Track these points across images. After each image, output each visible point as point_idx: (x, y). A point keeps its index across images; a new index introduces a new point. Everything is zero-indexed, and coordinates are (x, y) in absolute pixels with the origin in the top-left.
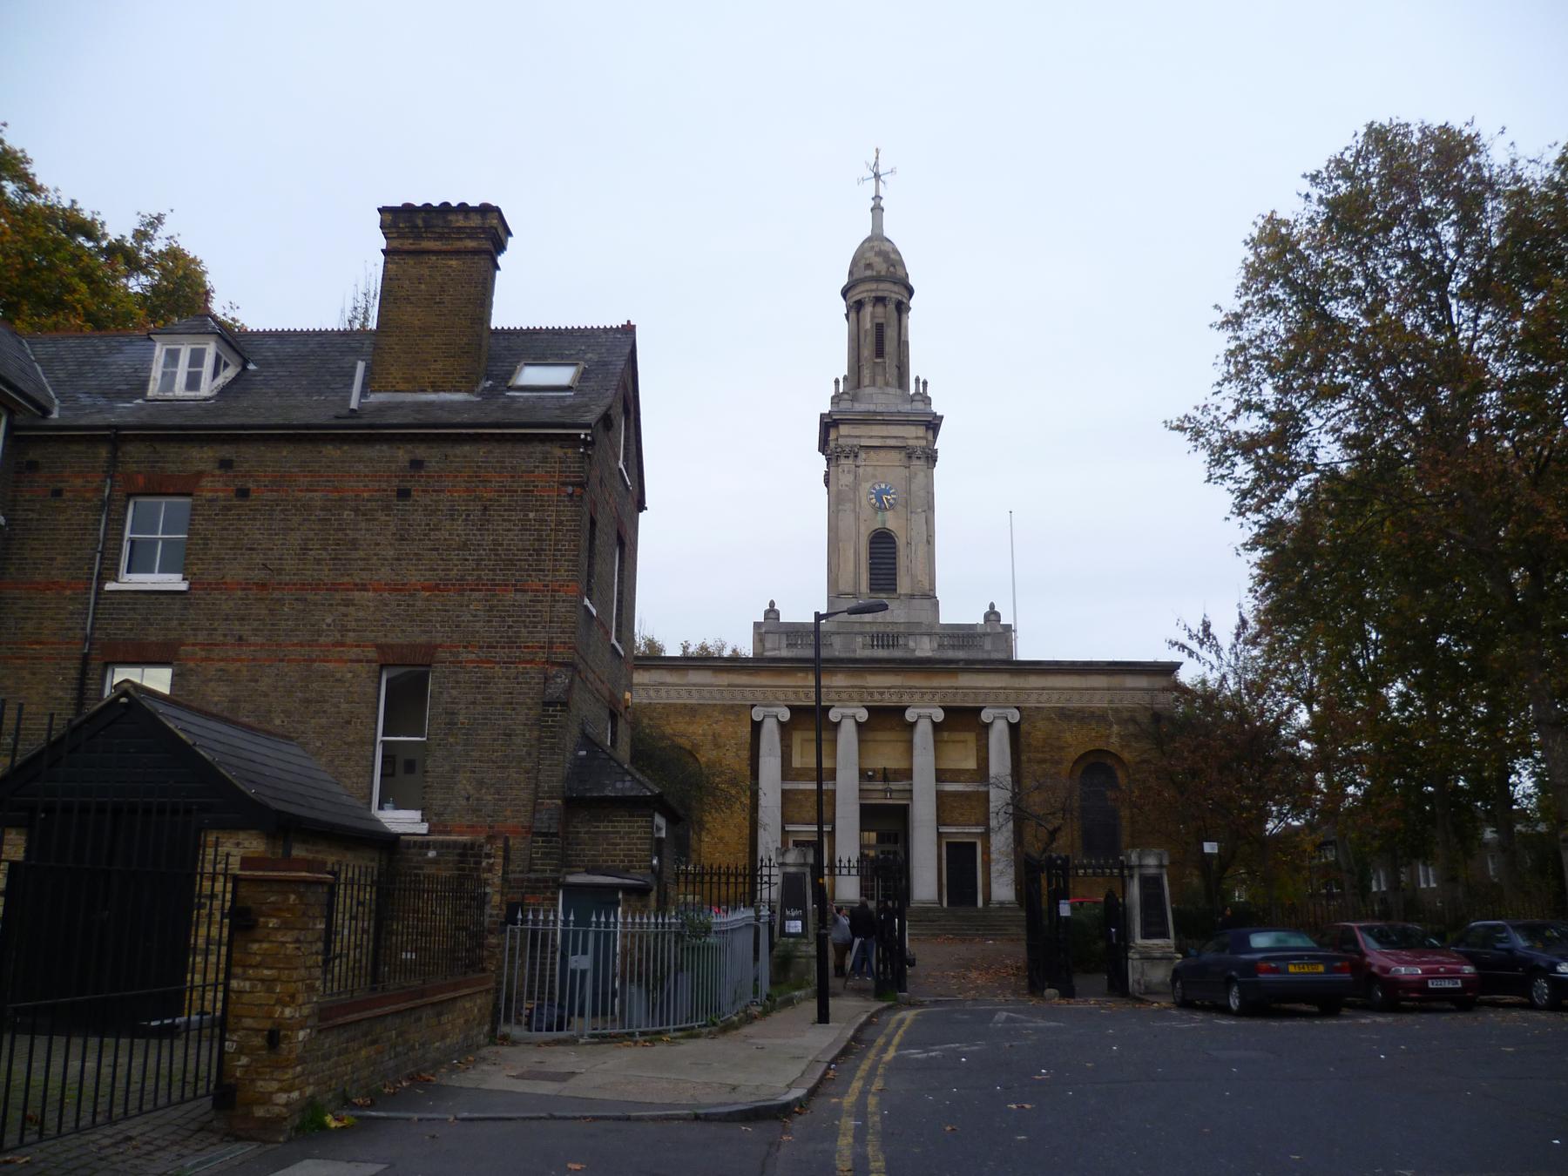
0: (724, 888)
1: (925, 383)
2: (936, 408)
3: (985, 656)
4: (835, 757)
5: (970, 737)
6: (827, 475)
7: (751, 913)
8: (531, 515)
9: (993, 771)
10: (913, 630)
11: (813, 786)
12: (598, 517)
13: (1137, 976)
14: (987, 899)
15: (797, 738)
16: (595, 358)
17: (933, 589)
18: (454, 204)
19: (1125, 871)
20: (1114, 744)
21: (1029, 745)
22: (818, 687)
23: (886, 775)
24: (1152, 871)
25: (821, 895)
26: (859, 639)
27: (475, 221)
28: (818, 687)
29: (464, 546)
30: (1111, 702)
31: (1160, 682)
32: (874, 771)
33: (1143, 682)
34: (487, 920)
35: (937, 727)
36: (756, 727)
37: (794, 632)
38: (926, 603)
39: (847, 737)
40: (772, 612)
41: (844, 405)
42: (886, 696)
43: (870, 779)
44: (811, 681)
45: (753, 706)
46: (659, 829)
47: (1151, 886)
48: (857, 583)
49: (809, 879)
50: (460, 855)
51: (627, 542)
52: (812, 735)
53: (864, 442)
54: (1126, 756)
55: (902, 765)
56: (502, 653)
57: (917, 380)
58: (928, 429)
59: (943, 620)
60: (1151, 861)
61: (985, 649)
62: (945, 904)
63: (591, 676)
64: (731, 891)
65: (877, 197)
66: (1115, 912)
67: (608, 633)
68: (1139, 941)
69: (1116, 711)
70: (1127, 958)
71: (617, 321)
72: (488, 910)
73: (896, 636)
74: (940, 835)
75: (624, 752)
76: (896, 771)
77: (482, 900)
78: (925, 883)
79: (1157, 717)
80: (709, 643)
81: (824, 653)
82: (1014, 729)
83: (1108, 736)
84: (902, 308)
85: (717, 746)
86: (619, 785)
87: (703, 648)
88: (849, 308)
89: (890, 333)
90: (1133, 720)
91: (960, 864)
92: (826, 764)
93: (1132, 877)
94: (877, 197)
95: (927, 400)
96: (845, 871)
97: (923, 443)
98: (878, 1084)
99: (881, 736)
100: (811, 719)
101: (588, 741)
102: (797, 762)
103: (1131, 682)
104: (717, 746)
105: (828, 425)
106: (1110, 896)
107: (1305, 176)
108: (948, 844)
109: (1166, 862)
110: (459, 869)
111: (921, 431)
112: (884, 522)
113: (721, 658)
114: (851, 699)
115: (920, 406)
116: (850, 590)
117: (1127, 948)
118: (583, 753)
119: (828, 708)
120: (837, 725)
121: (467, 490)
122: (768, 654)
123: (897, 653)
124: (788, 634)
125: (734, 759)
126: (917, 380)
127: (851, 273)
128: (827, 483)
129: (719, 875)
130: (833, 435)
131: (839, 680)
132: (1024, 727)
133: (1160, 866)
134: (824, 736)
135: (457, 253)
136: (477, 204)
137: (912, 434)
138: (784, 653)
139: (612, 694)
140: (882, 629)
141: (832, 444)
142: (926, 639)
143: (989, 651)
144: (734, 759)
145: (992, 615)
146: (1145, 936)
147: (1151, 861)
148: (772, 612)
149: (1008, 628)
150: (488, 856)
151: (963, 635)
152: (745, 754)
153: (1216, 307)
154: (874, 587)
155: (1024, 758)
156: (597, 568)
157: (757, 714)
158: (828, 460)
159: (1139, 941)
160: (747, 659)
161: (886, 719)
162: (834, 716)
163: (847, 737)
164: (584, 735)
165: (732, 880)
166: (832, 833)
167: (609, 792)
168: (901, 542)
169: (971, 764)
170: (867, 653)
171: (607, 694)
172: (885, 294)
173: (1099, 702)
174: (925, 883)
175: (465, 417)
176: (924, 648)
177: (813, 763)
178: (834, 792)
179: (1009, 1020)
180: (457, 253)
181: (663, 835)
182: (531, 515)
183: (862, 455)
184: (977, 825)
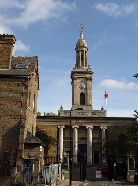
0: (54, 160)
5: (98, 132)
6: (72, 82)
7: (58, 165)
8: (19, 92)
9: (102, 138)
10: (88, 112)
11: (69, 141)
12: (31, 92)
14: (101, 162)
15: (66, 131)
16: (31, 63)
18: (6, 35)
19: (126, 158)
20: (125, 133)
21: (109, 133)
25: (71, 162)
26: (78, 113)
27: (9, 38)
29: (6, 97)
30: (124, 125)
31: (133, 121)
33: (130, 121)
34: (10, 166)
35: (92, 130)
37: (66, 111)
40: (61, 108)
41: (75, 70)
45: (58, 125)
46: (41, 149)
47: (131, 160)
48: (77, 102)
49: (68, 158)
50: (5, 154)
51: (36, 96)
52: (69, 131)
54: (127, 135)
55: (86, 137)
56: (13, 117)
59: (93, 110)
60: (131, 155)
61: (100, 117)
63: (29, 121)
64: (51, 161)
66: (125, 164)
67: (32, 113)
69: (125, 127)
70: (127, 174)
71: (35, 56)
72: (10, 164)
73: (84, 113)
74: (92, 150)
75: (34, 134)
76: (84, 138)
77: (9, 162)
78: (90, 158)
79: (133, 128)
80: (49, 113)
81: (72, 116)
82: (106, 130)
83: (124, 132)
85: (51, 133)
86: (34, 141)
87: (48, 114)
90: (128, 129)
91: (96, 155)
92: (71, 136)
93: (127, 158)
100: (69, 129)
101: (28, 133)
102: (66, 136)
103: (128, 121)
105: (72, 73)
106: (124, 162)
107: (134, 76)
108: (94, 152)
109: (134, 156)
110: (5, 156)
113: (51, 116)
118: (28, 135)
119: (72, 126)
121: (7, 87)
125: (54, 136)
127: (77, 45)
128: (72, 84)
129: (48, 158)
131: (74, 121)
133: (133, 156)
134: (71, 131)
135: (6, 44)
136: (10, 35)
139: (33, 124)
141: (73, 77)
144: (54, 136)
147: (131, 155)
148: (61, 108)
149: (105, 111)
150: (11, 154)
151: (97, 112)
152: (56, 134)
155: (108, 136)
156: (31, 101)
157: (59, 127)
158: (72, 80)
159: (129, 170)
160: (57, 117)
162: (73, 127)
164: (28, 132)
165: (54, 158)
166: (72, 149)
167: (32, 142)
168: (85, 95)
169: (98, 137)
170: (79, 116)
171: (32, 124)
173: (122, 125)
174: (90, 158)
175: (7, 74)
176: (90, 115)
177: (69, 136)
178: (73, 142)
179: (105, 185)
180: (6, 44)
181: (42, 150)
182: (19, 92)
184: (99, 148)
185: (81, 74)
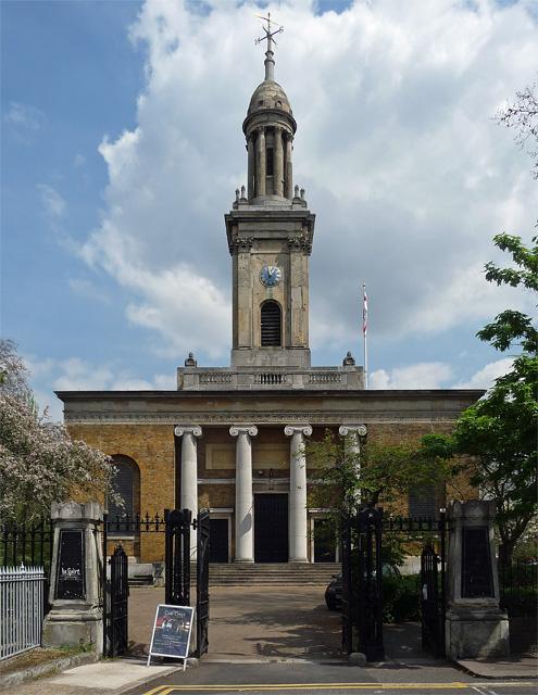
1: (303, 191)
2: (311, 208)
10: (293, 371)
13: (455, 639)
17: (307, 344)
23: (272, 474)
24: (477, 523)
32: (263, 470)
36: (179, 441)
37: (205, 374)
38: (301, 352)
40: (190, 361)
41: (242, 208)
43: (261, 476)
53: (257, 235)
55: (227, 466)
57: (296, 188)
58: (303, 225)
62: (313, 561)
65: (269, 52)
68: (458, 600)
70: (445, 618)
84: (287, 138)
89: (280, 155)
93: (452, 530)
94: (269, 52)
95: (304, 203)
96: (152, 528)
99: (268, 447)
100: (216, 439)
102: (209, 466)
105: (232, 222)
111: (299, 226)
112: (271, 295)
115: (298, 208)
117: (446, 607)
122: (185, 389)
123: (278, 387)
124: (201, 376)
126: (296, 188)
130: (234, 232)
137: (293, 231)
138: (197, 388)
143: (342, 384)
145: (349, 360)
148: (190, 361)
149: (360, 369)
154: (265, 342)
157: (179, 431)
159: (458, 600)
161: (270, 437)
163: (246, 449)
170: (257, 387)
176: (299, 384)
185: (265, 226)
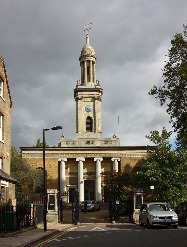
3: (113, 146)
4: (78, 170)
5: (109, 164)
22: (44, 154)
26: (83, 142)
28: (44, 154)
36: (60, 163)
39: (81, 165)
42: (89, 156)
44: (42, 152)
45: (58, 158)
55: (75, 171)
62: (103, 202)
82: (119, 162)
85: (50, 167)
88: (81, 63)
97: (98, 96)
98: (44, 244)
104: (50, 167)
114: (81, 156)
116: (81, 131)
120: (96, 162)
127: (81, 54)
132: (121, 162)
140: (89, 140)
142: (99, 142)
146: (136, 209)
153: (165, 61)
172: (89, 59)
183: (84, 99)
